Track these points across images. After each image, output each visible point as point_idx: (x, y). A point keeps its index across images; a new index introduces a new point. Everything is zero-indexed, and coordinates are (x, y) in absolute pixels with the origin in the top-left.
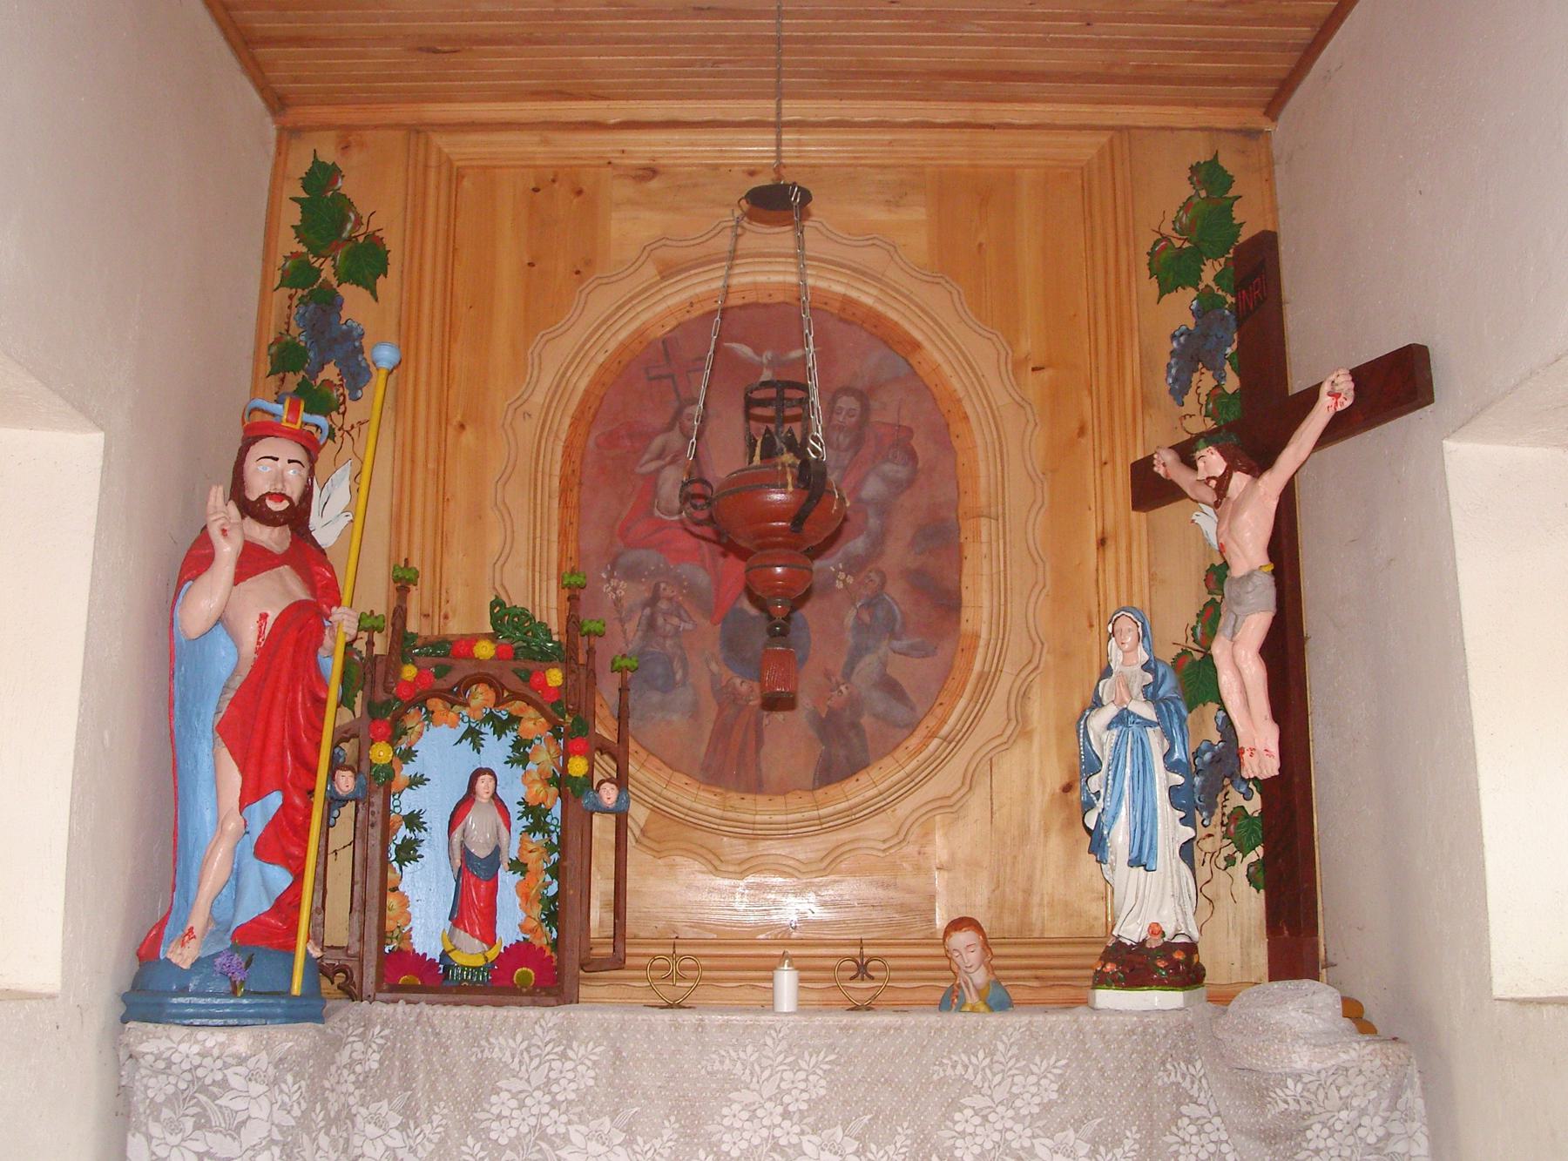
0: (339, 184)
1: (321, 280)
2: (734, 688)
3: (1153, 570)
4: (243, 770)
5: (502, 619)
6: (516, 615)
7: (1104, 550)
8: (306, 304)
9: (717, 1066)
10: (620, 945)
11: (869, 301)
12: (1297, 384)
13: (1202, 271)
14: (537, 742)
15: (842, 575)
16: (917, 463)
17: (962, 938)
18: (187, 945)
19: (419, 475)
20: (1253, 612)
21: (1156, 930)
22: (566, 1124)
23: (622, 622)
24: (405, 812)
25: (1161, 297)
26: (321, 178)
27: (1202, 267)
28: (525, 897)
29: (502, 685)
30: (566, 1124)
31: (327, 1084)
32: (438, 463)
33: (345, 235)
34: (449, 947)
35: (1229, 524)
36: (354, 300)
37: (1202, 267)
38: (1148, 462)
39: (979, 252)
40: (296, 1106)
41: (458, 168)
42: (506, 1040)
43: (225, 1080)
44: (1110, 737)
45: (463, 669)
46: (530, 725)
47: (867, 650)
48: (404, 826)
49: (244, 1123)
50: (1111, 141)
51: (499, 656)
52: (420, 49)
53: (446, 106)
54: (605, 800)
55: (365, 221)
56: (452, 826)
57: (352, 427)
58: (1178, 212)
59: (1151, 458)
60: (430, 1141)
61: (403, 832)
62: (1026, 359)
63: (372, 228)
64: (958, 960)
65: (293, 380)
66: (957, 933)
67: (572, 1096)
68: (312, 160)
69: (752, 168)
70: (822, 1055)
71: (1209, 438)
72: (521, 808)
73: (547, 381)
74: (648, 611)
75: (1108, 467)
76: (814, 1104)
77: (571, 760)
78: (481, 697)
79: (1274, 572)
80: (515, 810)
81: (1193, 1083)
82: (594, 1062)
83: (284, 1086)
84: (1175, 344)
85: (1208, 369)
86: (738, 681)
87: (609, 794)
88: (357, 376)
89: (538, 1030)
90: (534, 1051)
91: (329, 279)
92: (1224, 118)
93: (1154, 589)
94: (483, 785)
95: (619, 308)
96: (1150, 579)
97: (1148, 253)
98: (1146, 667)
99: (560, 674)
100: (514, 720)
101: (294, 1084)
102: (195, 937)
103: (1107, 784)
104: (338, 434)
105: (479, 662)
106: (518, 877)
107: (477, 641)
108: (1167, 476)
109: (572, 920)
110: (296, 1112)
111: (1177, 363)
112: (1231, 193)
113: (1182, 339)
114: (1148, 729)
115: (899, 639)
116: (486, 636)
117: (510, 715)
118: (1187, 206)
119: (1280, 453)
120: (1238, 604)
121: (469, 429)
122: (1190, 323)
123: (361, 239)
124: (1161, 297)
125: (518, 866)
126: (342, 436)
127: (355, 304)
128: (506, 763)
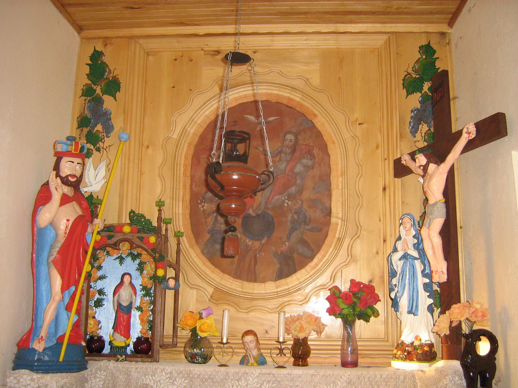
0: (103, 59)
1: (96, 94)
2: (246, 243)
4: (62, 277)
5: (134, 218)
6: (139, 217)
7: (385, 192)
8: (91, 103)
9: (144, 382)
10: (175, 339)
11: (298, 99)
12: (455, 129)
13: (424, 86)
14: (148, 263)
15: (287, 201)
16: (315, 160)
17: (249, 338)
18: (41, 343)
20: (437, 218)
24: (98, 289)
25: (407, 96)
26: (96, 56)
27: (424, 84)
28: (142, 320)
33: (105, 77)
34: (112, 339)
35: (428, 183)
36: (107, 100)
37: (424, 84)
38: (399, 159)
42: (152, 376)
45: (118, 237)
46: (145, 256)
47: (296, 229)
48: (97, 294)
50: (389, 37)
51: (132, 232)
52: (127, 8)
53: (141, 29)
54: (170, 285)
55: (112, 72)
56: (114, 294)
57: (107, 147)
58: (414, 64)
59: (400, 158)
61: (97, 296)
62: (356, 120)
63: (115, 74)
64: (247, 346)
65: (86, 130)
66: (247, 336)
68: (94, 50)
69: (255, 50)
71: (421, 150)
72: (141, 287)
73: (178, 130)
75: (387, 161)
78: (125, 247)
79: (445, 202)
80: (138, 288)
84: (413, 114)
86: (248, 240)
87: (172, 283)
88: (108, 128)
91: (99, 93)
92: (432, 28)
93: (403, 207)
94: (126, 279)
95: (205, 103)
98: (414, 237)
99: (155, 238)
100: (139, 255)
102: (43, 340)
103: (399, 282)
104: (102, 150)
105: (125, 234)
106: (139, 313)
107: (124, 226)
108: (406, 165)
109: (158, 329)
112: (435, 57)
113: (415, 112)
114: (415, 261)
115: (308, 225)
118: (418, 61)
119: (448, 155)
120: (431, 215)
122: (419, 106)
123: (111, 79)
124: (407, 96)
125: (139, 309)
126: (103, 151)
127: (108, 102)
128: (136, 270)
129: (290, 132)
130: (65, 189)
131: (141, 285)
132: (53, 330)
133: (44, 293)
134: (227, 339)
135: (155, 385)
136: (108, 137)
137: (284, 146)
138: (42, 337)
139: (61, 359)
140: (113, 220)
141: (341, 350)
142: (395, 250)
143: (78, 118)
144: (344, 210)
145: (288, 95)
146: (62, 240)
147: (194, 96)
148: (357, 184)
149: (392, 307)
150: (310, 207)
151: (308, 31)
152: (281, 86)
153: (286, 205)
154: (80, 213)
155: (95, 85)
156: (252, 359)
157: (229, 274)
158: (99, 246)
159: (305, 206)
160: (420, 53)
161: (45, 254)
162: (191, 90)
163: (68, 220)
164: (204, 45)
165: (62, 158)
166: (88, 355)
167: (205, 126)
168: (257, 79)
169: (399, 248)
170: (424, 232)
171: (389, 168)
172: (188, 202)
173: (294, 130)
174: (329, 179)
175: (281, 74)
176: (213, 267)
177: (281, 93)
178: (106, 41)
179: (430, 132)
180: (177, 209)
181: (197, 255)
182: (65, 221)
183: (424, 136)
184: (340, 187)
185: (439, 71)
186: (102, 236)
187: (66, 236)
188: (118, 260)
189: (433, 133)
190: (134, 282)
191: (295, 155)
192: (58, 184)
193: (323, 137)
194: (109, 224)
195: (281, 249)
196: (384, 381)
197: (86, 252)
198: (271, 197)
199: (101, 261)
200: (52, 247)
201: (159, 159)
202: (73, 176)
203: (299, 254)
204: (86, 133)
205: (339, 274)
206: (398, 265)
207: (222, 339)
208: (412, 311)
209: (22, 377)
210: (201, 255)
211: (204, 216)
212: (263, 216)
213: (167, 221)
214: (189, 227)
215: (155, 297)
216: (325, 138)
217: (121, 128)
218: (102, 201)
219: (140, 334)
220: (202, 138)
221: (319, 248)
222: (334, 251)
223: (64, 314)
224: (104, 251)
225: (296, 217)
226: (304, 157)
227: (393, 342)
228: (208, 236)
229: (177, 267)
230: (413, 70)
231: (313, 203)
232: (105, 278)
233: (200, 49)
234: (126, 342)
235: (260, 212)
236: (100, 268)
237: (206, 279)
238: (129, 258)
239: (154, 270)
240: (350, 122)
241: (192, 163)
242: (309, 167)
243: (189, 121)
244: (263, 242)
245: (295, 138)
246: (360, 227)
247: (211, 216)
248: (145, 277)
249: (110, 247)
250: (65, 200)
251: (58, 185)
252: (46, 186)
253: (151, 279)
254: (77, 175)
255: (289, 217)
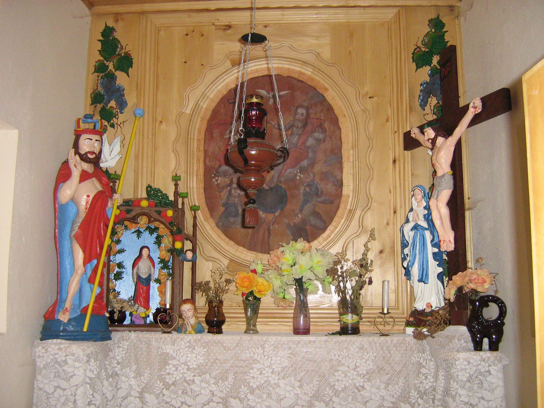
3: (413, 172)
4: (84, 251)
5: (151, 192)
9: (248, 355)
11: (309, 73)
14: (165, 236)
15: (299, 174)
19: (145, 141)
21: (429, 305)
22: (278, 380)
23: (219, 192)
24: (117, 262)
25: (417, 69)
26: (108, 32)
29: (150, 216)
30: (278, 380)
31: (107, 363)
32: (153, 136)
33: (117, 53)
35: (436, 156)
36: (120, 76)
39: (350, 54)
40: (95, 371)
41: (158, 27)
42: (255, 350)
43: (66, 361)
44: (412, 234)
46: (162, 230)
49: (72, 377)
50: (399, 11)
51: (150, 205)
55: (124, 48)
56: (134, 266)
57: (121, 123)
59: (410, 131)
60: (144, 383)
61: (117, 269)
65: (99, 106)
67: (195, 366)
70: (286, 351)
71: (430, 124)
73: (191, 105)
74: (229, 188)
75: (397, 134)
76: (284, 368)
77: (176, 243)
78: (143, 221)
79: (453, 174)
80: (156, 261)
81: (258, 356)
82: (203, 354)
83: (90, 363)
84: (422, 87)
85: (434, 97)
87: (189, 255)
88: (122, 105)
89: (183, 343)
90: (266, 354)
93: (413, 179)
95: (217, 78)
96: (412, 175)
97: (412, 53)
98: (425, 208)
99: (172, 212)
100: (156, 229)
101: (94, 362)
104: (116, 126)
105: (143, 208)
106: (158, 285)
110: (95, 372)
111: (422, 94)
112: (444, 30)
113: (425, 85)
115: (319, 198)
116: (145, 199)
117: (155, 227)
118: (427, 35)
120: (439, 186)
121: (164, 123)
122: (428, 79)
123: (123, 55)
124: (417, 69)
125: (158, 281)
126: (117, 127)
127: (121, 78)
128: (154, 243)
129: (301, 106)
130: (84, 165)
131: (159, 258)
132: (78, 302)
133: (68, 266)
134: (388, 310)
135: (344, 359)
136: (122, 113)
137: (296, 120)
138: (67, 309)
139: (85, 329)
140: (130, 196)
141: (294, 318)
142: (407, 221)
143: (91, 94)
144: (355, 182)
145: (299, 69)
146: (83, 215)
147: (206, 71)
148: (368, 157)
149: (405, 276)
150: (322, 180)
151: (318, 5)
152: (291, 60)
153: (298, 178)
154: (100, 188)
155: (107, 61)
156: (190, 327)
157: (244, 246)
158: (119, 221)
159: (317, 179)
160: (429, 26)
161: (68, 229)
162: (202, 65)
163: (88, 196)
164: (215, 19)
165: (81, 135)
166: (110, 326)
167: (217, 100)
168: (239, 53)
169: (411, 219)
170: (432, 203)
171: (399, 140)
172: (202, 177)
173: (305, 104)
174: (340, 152)
175: (292, 48)
176: (227, 240)
177: (292, 67)
178: (117, 17)
179: (438, 105)
180: (191, 183)
181: (212, 228)
182: (85, 197)
183: (433, 109)
184: (351, 160)
185: (448, 44)
186: (121, 211)
187: (87, 211)
188: (135, 234)
189: (442, 106)
190: (151, 255)
191: (307, 128)
192: (77, 161)
193: (335, 111)
194: (127, 199)
195: (294, 221)
196: (395, 346)
197: (107, 226)
198: (283, 170)
199: (120, 235)
200: (74, 223)
201: (173, 133)
202: (93, 153)
203: (312, 226)
204: (100, 109)
205: (351, 245)
206: (409, 235)
207: (383, 309)
208: (423, 279)
209: (50, 347)
210: (216, 228)
211: (218, 190)
212: (275, 189)
213: (183, 195)
214: (203, 200)
215: (173, 269)
216: (336, 112)
217: (134, 103)
218: (120, 176)
219: (159, 305)
220: (215, 112)
221: (331, 220)
222: (345, 222)
223: (87, 287)
224: (123, 225)
225: (308, 190)
226: (315, 130)
227: (403, 310)
228: (222, 209)
229: (193, 239)
230: (422, 44)
231: (324, 176)
232: (123, 252)
233: (212, 24)
234: (146, 313)
235: (273, 186)
236: (118, 242)
237: (221, 251)
238: (147, 232)
239: (172, 243)
240: (360, 96)
241: (205, 138)
242: (320, 140)
243: (201, 96)
244: (277, 214)
245: (306, 112)
246: (371, 199)
247: (225, 191)
248: (163, 250)
249: (129, 221)
250: (84, 176)
251: (77, 163)
252: (66, 163)
253: (169, 252)
254: (95, 151)
255: (302, 191)
